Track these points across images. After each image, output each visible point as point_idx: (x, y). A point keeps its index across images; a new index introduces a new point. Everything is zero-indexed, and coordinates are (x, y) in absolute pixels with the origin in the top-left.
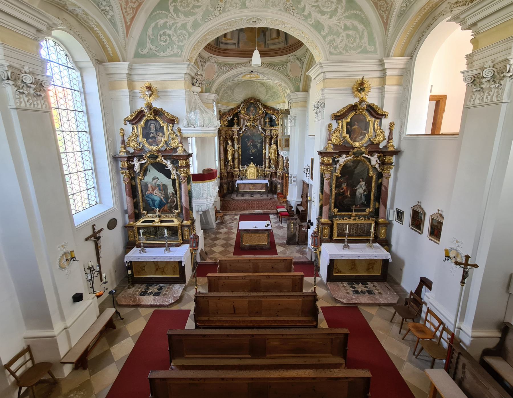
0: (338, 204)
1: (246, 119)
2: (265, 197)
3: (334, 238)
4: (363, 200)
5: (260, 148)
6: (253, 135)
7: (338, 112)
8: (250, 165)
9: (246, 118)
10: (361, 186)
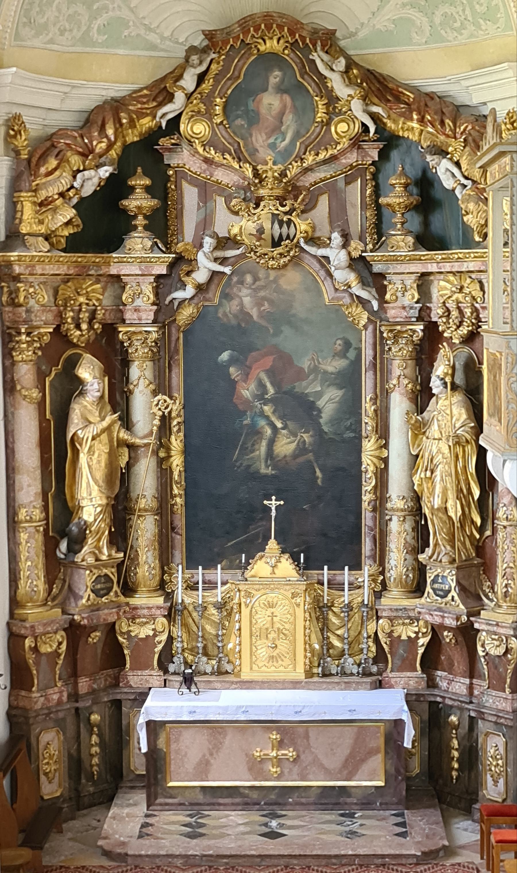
1: (221, 189)
2: (377, 835)
5: (335, 421)
6: (282, 316)
8: (260, 568)
9: (221, 176)
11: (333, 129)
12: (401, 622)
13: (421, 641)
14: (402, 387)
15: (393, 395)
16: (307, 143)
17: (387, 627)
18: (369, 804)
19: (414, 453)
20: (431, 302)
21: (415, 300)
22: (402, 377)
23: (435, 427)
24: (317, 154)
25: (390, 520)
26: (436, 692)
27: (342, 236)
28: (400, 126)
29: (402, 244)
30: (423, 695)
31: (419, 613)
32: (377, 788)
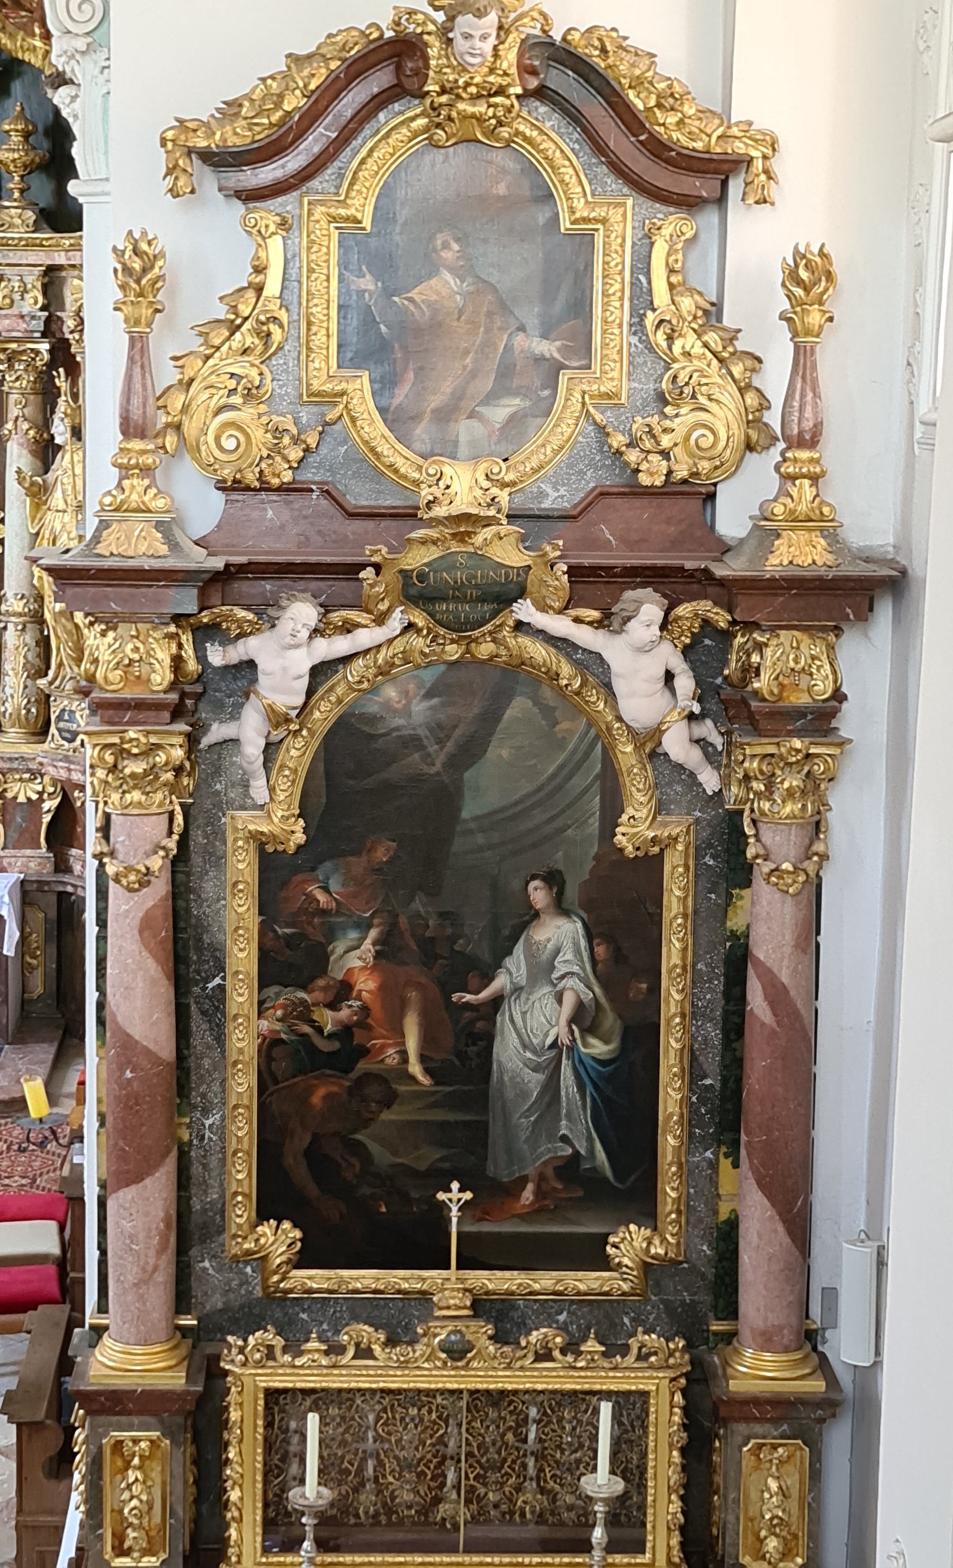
0: (301, 1173)
4: (578, 1131)
7: (231, 109)
10: (542, 970)
12: (17, 777)
13: (46, 806)
14: (20, 434)
15: (9, 444)
19: (34, 531)
20: (63, 310)
21: (39, 306)
22: (21, 419)
23: (58, 494)
26: (67, 878)
28: (18, 44)
29: (18, 221)
30: (48, 883)
31: (41, 764)
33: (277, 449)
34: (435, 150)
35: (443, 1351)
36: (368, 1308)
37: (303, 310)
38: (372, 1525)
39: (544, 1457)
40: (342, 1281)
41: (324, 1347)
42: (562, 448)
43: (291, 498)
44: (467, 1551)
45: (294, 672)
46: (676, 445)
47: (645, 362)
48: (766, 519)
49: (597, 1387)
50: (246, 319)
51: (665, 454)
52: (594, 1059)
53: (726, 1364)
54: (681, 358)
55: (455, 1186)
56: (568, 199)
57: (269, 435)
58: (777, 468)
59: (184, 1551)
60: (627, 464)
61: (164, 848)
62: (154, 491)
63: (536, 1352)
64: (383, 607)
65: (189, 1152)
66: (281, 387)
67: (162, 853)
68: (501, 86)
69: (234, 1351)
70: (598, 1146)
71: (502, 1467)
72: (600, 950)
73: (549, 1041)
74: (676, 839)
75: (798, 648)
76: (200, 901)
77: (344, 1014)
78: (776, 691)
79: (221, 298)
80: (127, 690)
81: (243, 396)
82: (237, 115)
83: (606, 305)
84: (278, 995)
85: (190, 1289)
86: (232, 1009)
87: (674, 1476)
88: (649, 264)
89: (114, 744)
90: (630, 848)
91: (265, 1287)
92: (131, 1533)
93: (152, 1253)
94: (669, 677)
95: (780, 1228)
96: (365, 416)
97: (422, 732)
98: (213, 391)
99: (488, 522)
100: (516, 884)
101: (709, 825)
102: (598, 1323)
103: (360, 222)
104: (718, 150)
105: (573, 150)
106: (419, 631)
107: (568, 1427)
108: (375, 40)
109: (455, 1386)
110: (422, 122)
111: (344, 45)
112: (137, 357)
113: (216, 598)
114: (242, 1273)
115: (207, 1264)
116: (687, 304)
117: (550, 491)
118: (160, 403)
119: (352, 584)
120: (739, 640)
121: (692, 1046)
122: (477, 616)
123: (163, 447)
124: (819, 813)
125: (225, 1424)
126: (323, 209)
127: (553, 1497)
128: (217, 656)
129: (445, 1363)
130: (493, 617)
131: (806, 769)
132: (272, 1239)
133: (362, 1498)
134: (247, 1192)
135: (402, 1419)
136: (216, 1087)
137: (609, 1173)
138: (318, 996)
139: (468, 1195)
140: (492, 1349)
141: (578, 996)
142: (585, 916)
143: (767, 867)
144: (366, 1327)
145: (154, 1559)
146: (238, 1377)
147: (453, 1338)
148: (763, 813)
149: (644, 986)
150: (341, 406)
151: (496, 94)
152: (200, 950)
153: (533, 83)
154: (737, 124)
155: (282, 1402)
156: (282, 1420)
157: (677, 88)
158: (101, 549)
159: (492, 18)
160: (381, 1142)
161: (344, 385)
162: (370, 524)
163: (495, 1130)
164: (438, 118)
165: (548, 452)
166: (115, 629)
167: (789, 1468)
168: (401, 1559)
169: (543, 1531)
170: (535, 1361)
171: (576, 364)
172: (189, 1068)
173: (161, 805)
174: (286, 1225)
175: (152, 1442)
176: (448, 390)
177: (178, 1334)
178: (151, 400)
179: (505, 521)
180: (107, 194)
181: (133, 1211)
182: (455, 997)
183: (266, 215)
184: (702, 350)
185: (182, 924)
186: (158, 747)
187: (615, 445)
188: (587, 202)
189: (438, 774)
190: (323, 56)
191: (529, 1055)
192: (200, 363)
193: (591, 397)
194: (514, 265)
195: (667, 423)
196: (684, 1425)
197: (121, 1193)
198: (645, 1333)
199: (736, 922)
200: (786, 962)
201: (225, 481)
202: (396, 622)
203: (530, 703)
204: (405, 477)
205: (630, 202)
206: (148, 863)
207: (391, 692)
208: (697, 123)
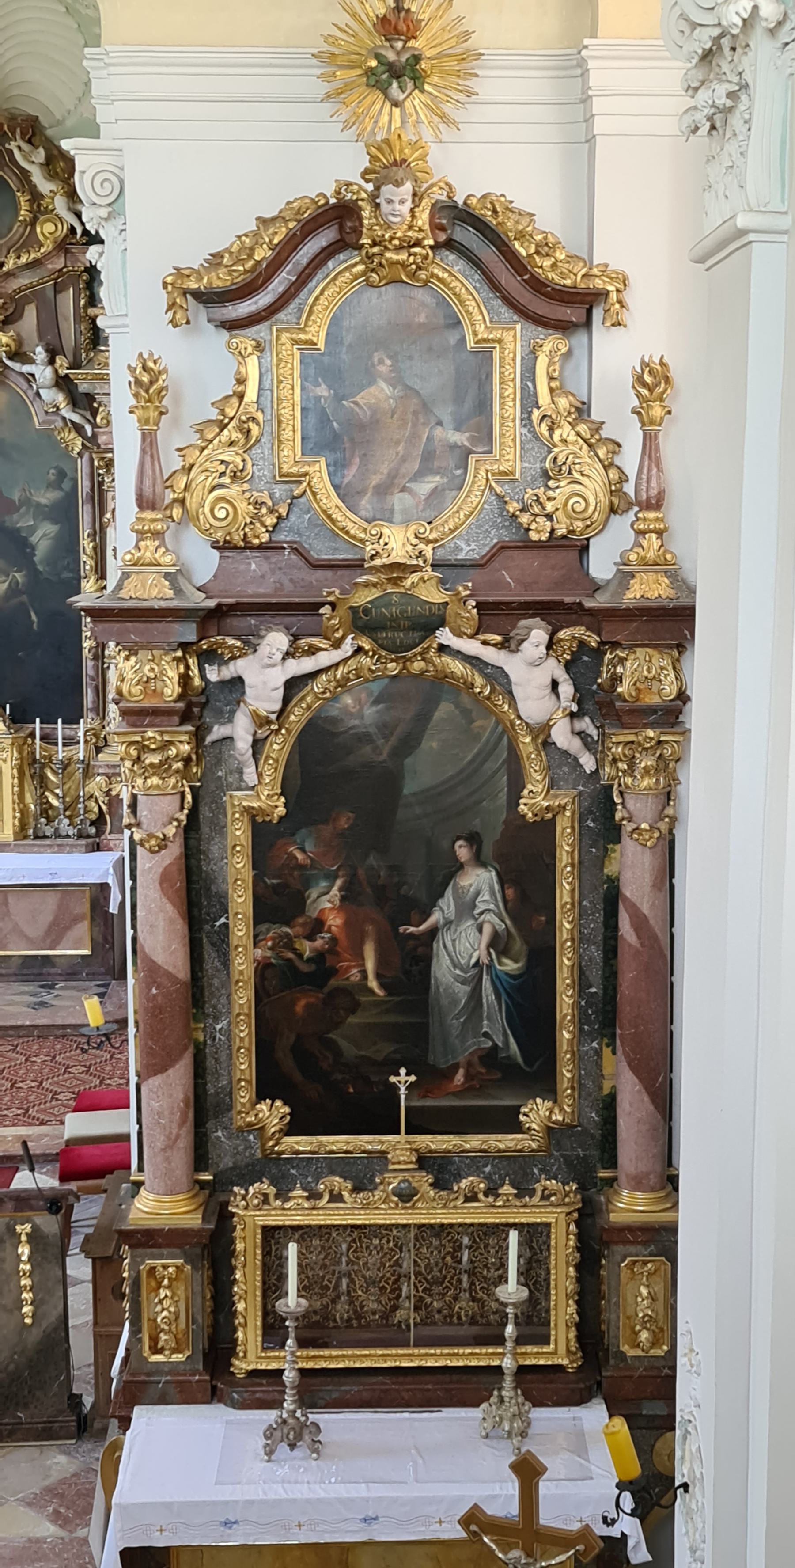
0: (288, 1064)
3: (241, 1366)
4: (496, 1029)
5: (51, 560)
7: (215, 261)
10: (467, 908)
11: (38, 230)
15: (108, 529)
16: (10, 244)
17: (104, 785)
18: (74, 974)
24: (19, 257)
25: (108, 668)
27: (47, 351)
32: (83, 957)
33: (257, 517)
34: (372, 289)
35: (395, 1195)
36: (340, 1165)
37: (275, 412)
38: (346, 1327)
39: (474, 1274)
40: (321, 1144)
41: (306, 1194)
42: (472, 513)
43: (269, 554)
44: (416, 1345)
45: (272, 685)
46: (557, 509)
47: (533, 448)
48: (625, 564)
49: (511, 1220)
50: (232, 419)
51: (549, 517)
52: (507, 974)
53: (609, 1201)
54: (559, 444)
55: (403, 1071)
56: (472, 325)
57: (251, 507)
58: (632, 526)
59: (204, 1349)
60: (521, 524)
61: (177, 820)
62: (163, 549)
63: (465, 1196)
64: (338, 635)
65: (204, 1049)
66: (259, 471)
67: (175, 823)
68: (418, 239)
69: (239, 1198)
70: (511, 1039)
71: (443, 1282)
72: (510, 892)
73: (473, 961)
74: (564, 808)
75: (650, 661)
76: (209, 860)
77: (319, 943)
78: (634, 694)
79: (213, 404)
80: (146, 701)
81: (231, 477)
82: (220, 264)
83: (502, 404)
84: (268, 931)
85: (207, 1153)
86: (234, 941)
87: (571, 1286)
88: (534, 373)
89: (138, 742)
90: (530, 815)
91: (264, 1150)
92: (163, 1337)
93: (175, 1125)
94: (555, 685)
95: (646, 1098)
96: (323, 491)
97: (372, 730)
98: (208, 474)
99: (415, 569)
100: (445, 844)
101: (589, 796)
102: (515, 1173)
103: (316, 344)
104: (583, 286)
105: (475, 287)
106: (366, 653)
107: (492, 1251)
108: (323, 205)
109: (405, 1222)
110: (361, 268)
111: (299, 209)
112: (148, 449)
113: (213, 630)
114: (246, 1140)
115: (220, 1134)
116: (563, 402)
117: (464, 546)
118: (168, 484)
119: (315, 618)
120: (608, 656)
121: (580, 963)
122: (410, 641)
123: (171, 517)
124: (670, 785)
125: (232, 1253)
126: (288, 335)
127: (481, 1303)
128: (213, 674)
129: (397, 1204)
130: (422, 641)
131: (658, 753)
132: (267, 1114)
133: (339, 1307)
134: (248, 1078)
135: (368, 1247)
136: (223, 1000)
137: (520, 1060)
138: (299, 930)
139: (413, 1078)
140: (432, 1193)
141: (494, 927)
142: (497, 866)
143: (633, 826)
144: (337, 1179)
145: (180, 1356)
146: (241, 1218)
147: (402, 1185)
148: (627, 787)
149: (543, 918)
150: (305, 484)
151: (414, 245)
152: (209, 897)
153: (442, 237)
154: (597, 266)
155: (277, 1236)
156: (277, 1249)
157: (551, 239)
158: (123, 594)
159: (408, 187)
160: (349, 1039)
161: (306, 469)
162: (329, 574)
163: (434, 1030)
164: (372, 264)
165: (462, 516)
166: (136, 654)
167: (656, 1278)
168: (367, 1352)
169: (475, 1330)
170: (464, 1202)
171: (480, 450)
172: (203, 986)
173: (174, 787)
174: (278, 1103)
175: (177, 1267)
176: (385, 471)
177: (197, 1187)
178: (159, 481)
179: (429, 569)
180: (126, 326)
181: (160, 1094)
182: (402, 929)
183: (245, 340)
184: (575, 438)
185: (195, 878)
186: (171, 743)
187: (511, 510)
188: (486, 327)
189: (384, 761)
190: (284, 218)
191: (458, 972)
192: (198, 453)
193: (493, 475)
194: (433, 376)
195: (551, 493)
196: (577, 1247)
197: (150, 1081)
198: (546, 1179)
199: (610, 869)
200: (646, 899)
201: (218, 542)
202: (348, 647)
203: (452, 707)
204: (354, 537)
205: (518, 327)
206: (165, 831)
207: (348, 700)
208: (566, 265)
